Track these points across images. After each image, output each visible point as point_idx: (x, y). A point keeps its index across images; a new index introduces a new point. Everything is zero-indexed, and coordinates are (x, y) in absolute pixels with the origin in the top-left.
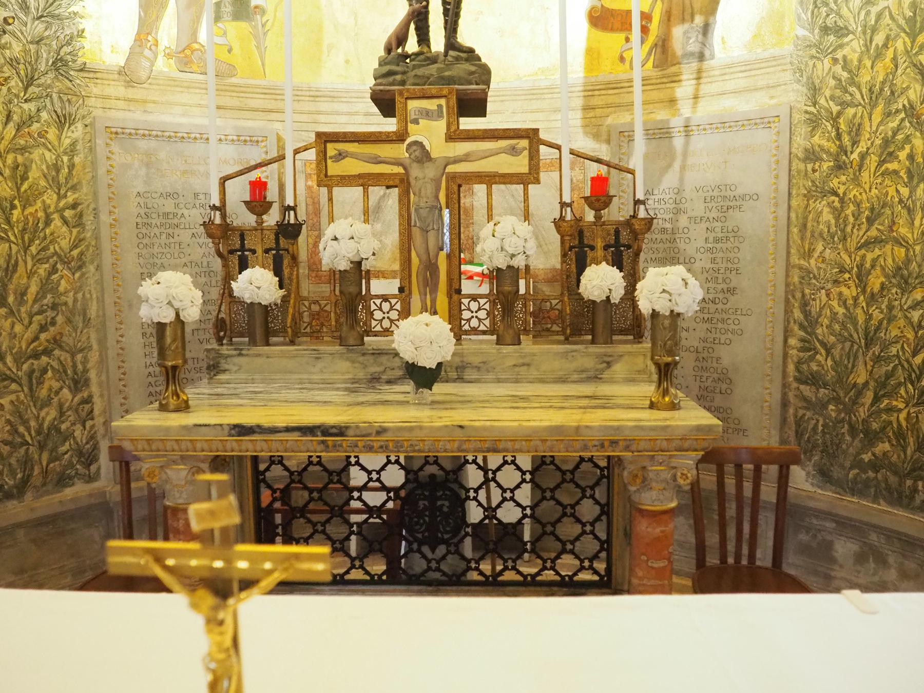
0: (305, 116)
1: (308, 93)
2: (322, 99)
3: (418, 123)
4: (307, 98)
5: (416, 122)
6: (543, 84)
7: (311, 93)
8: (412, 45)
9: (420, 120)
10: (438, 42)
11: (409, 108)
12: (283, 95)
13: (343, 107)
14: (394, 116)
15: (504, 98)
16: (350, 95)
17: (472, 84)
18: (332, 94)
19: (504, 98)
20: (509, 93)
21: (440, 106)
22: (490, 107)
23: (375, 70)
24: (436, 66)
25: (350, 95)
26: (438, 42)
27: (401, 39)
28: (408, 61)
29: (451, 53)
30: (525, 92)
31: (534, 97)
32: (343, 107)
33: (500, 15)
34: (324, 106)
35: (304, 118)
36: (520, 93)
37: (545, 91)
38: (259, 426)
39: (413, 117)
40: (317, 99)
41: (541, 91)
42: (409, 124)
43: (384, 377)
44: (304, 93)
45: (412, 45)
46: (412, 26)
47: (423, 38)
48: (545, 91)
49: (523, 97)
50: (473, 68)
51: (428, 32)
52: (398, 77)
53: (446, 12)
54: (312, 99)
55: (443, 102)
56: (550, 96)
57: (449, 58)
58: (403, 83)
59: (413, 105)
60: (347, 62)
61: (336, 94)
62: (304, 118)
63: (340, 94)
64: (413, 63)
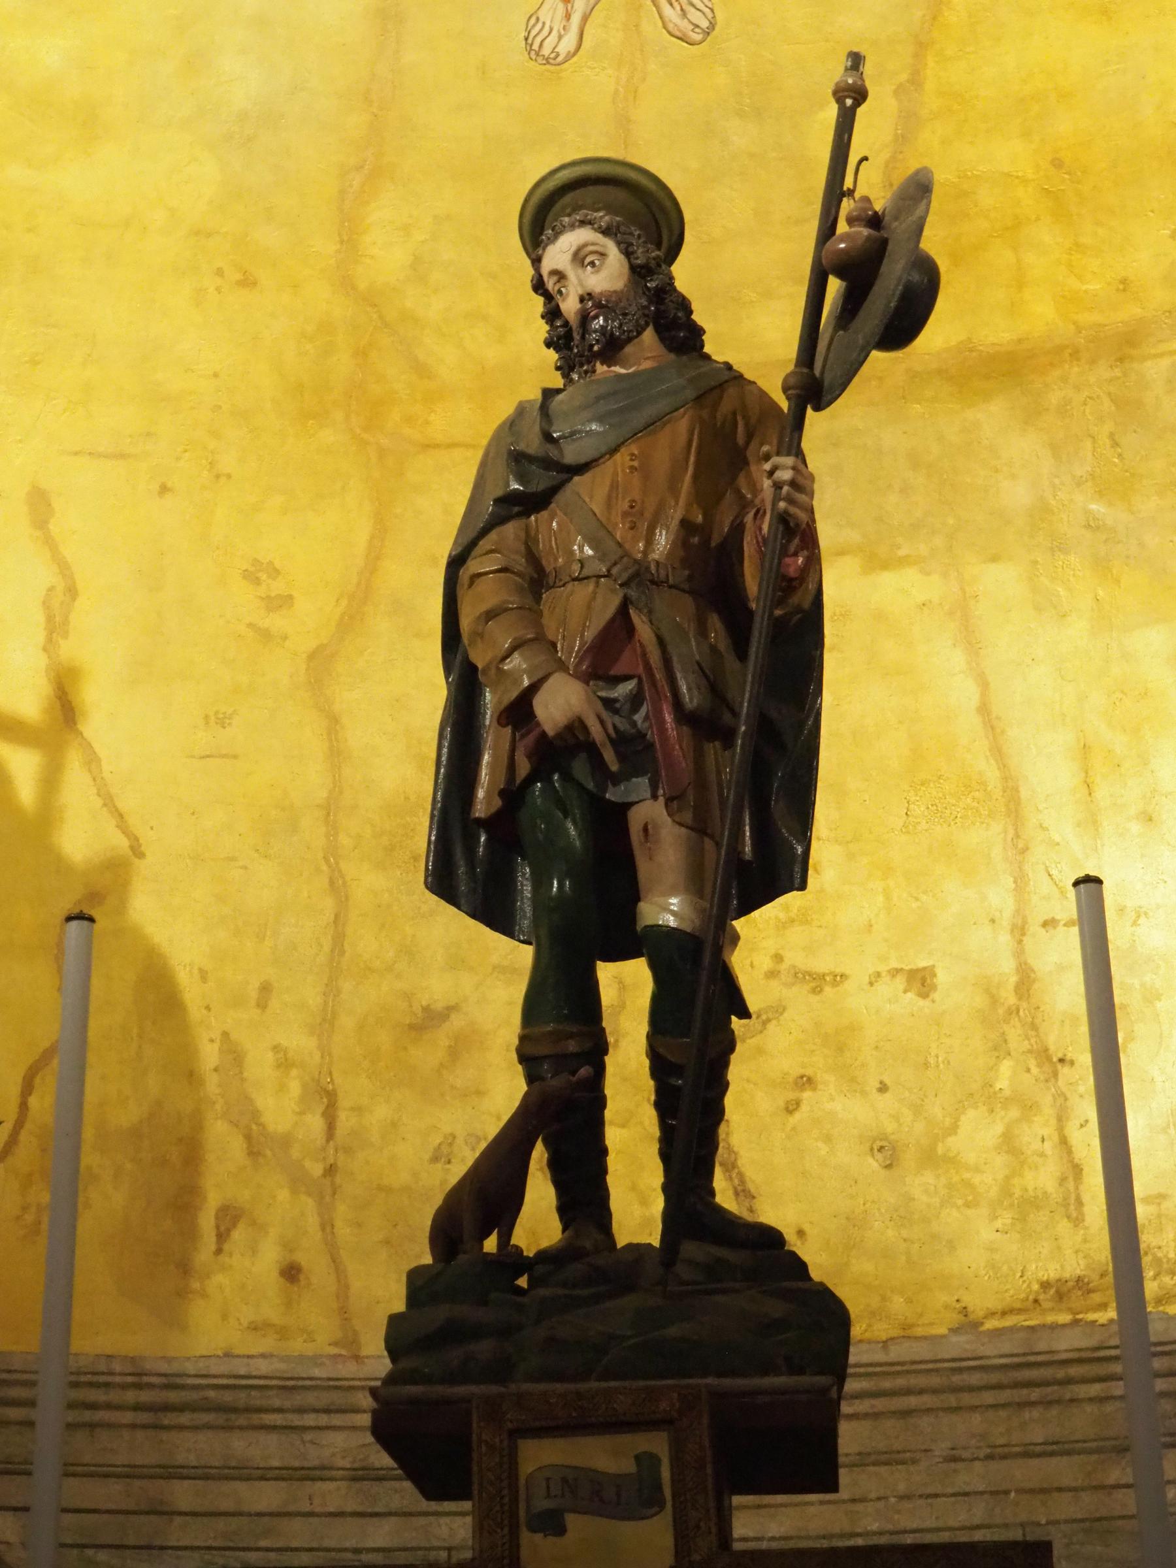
0: (115, 1488)
1: (130, 1396)
2: (185, 1418)
3: (561, 1531)
4: (128, 1417)
5: (552, 1523)
6: (1065, 1344)
7: (145, 1397)
8: (539, 1220)
9: (571, 1519)
10: (637, 1204)
11: (527, 1468)
12: (31, 1403)
13: (267, 1449)
14: (466, 1496)
15: (913, 1401)
16: (298, 1399)
17: (766, 1370)
18: (227, 1397)
19: (913, 1401)
20: (935, 1381)
21: (646, 1461)
22: (851, 1437)
23: (394, 1321)
24: (630, 1302)
25: (298, 1399)
26: (637, 1204)
27: (489, 1192)
28: (523, 1282)
29: (691, 1249)
30: (994, 1378)
31: (1035, 1394)
32: (267, 1449)
33: (883, 1088)
34: (192, 1447)
35: (109, 1494)
36: (975, 1379)
37: (1074, 1371)
38: (30, 1068)
39: (542, 1504)
40: (168, 1419)
41: (1061, 1373)
42: (526, 1537)
43: (1024, 1005)
44: (114, 1396)
45: (539, 1220)
46: (539, 1153)
47: (583, 1194)
48: (1074, 1371)
49: (989, 1397)
50: (776, 1308)
51: (604, 1171)
52: (484, 1348)
53: (665, 1104)
54: (144, 1417)
55: (658, 1444)
56: (1095, 1389)
57: (681, 1270)
58: (500, 1371)
59: (540, 1456)
60: (291, 1273)
61: (242, 1398)
62: (109, 1494)
63: (257, 1399)
64: (543, 1292)
